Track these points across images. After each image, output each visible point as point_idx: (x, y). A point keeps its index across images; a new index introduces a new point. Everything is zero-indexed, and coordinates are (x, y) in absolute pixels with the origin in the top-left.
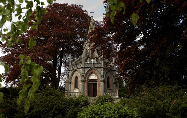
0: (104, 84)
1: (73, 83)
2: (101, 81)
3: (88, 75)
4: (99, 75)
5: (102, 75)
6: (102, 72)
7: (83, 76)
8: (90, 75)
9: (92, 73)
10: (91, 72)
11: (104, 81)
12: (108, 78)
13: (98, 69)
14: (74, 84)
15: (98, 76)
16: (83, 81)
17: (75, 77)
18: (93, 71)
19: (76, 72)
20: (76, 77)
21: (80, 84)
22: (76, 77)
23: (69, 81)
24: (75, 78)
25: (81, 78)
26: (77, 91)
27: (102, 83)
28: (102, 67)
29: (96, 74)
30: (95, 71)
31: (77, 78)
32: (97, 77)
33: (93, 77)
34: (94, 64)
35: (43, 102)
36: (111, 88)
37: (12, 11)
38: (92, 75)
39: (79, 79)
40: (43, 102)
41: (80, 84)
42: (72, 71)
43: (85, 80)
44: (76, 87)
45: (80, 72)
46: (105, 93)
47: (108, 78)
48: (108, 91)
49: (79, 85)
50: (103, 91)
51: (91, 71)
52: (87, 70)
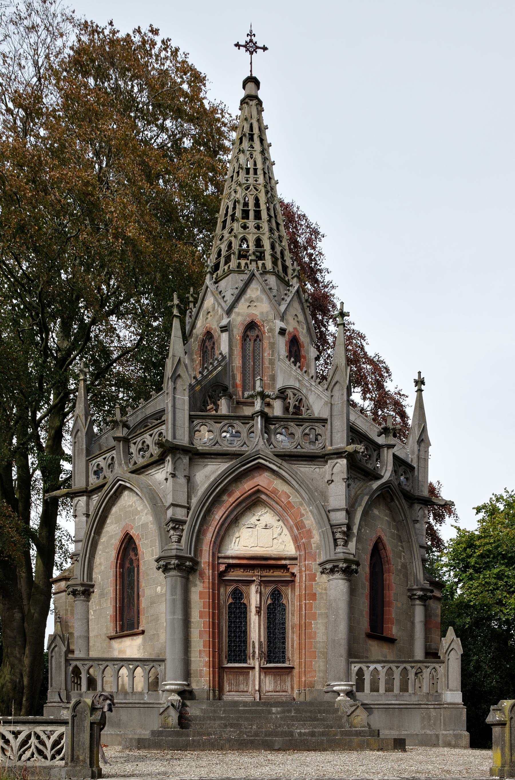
0: (352, 592)
1: (102, 595)
2: (330, 568)
3: (219, 514)
4: (310, 521)
5: (340, 517)
6: (337, 495)
7: (177, 524)
8: (232, 522)
9: (253, 501)
10: (238, 494)
11: (349, 570)
12: (377, 550)
13: (305, 470)
14: (112, 595)
15: (300, 525)
16: (183, 567)
17: (116, 542)
18: (262, 480)
19: (127, 499)
20: (128, 545)
21: (156, 589)
22: (128, 545)
23: (77, 573)
24: (113, 554)
25: (165, 539)
26: (131, 647)
27: (336, 587)
28: (338, 454)
29: (284, 512)
30: (286, 488)
31: (135, 549)
32: (295, 540)
33: (259, 536)
34: (266, 430)
35: (97, 94)
36: (394, 631)
37: (378, 365)
38: (251, 519)
39: (149, 552)
40: (97, 94)
41: (156, 589)
42: (96, 498)
43: (195, 562)
44: (127, 621)
45: (154, 499)
46: (355, 667)
47: (377, 550)
48: (376, 649)
49: (144, 603)
50: (343, 650)
51: (247, 486)
52: (208, 473)
